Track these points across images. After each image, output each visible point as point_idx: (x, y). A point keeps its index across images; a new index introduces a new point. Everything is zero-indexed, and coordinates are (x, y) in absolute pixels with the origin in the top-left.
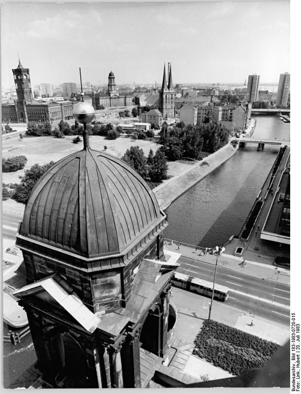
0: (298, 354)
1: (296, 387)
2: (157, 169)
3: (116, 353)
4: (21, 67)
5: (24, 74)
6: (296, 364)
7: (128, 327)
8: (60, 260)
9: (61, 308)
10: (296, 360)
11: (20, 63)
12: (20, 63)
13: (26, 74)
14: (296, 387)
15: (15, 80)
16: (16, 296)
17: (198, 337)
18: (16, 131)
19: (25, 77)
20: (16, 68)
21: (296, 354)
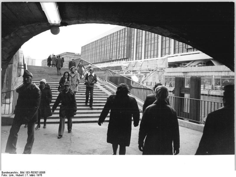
0: (24, 175)
3: (90, 107)
6: (18, 174)
8: (174, 147)
9: (106, 23)
10: (21, 174)
14: (4, 174)
18: (101, 85)
21: (24, 174)
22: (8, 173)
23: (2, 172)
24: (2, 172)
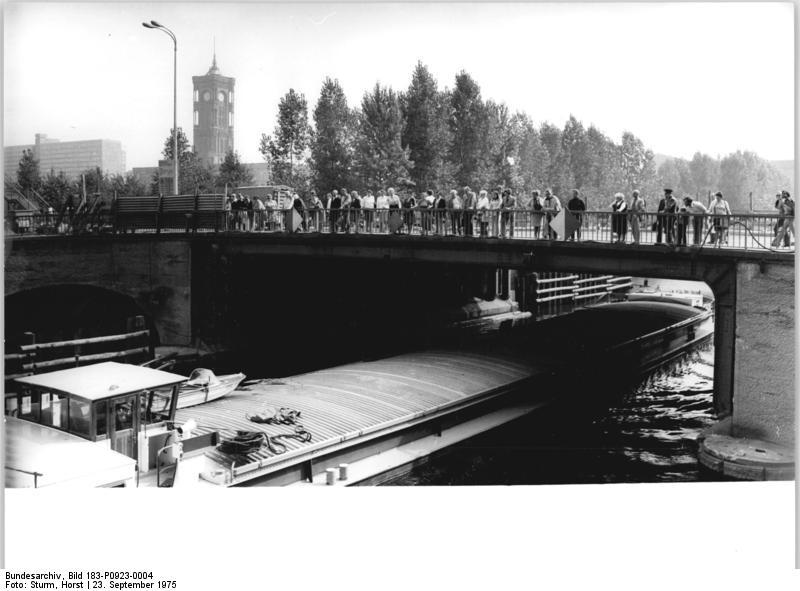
0: (85, 585)
1: (14, 581)
2: (549, 181)
4: (217, 72)
5: (219, 89)
7: (308, 161)
10: (70, 581)
11: (214, 63)
12: (214, 63)
13: (226, 91)
14: (14, 581)
15: (195, 103)
16: (252, 184)
17: (414, 82)
19: (221, 97)
20: (203, 72)
22: (28, 576)
23: (8, 575)
24: (8, 575)
